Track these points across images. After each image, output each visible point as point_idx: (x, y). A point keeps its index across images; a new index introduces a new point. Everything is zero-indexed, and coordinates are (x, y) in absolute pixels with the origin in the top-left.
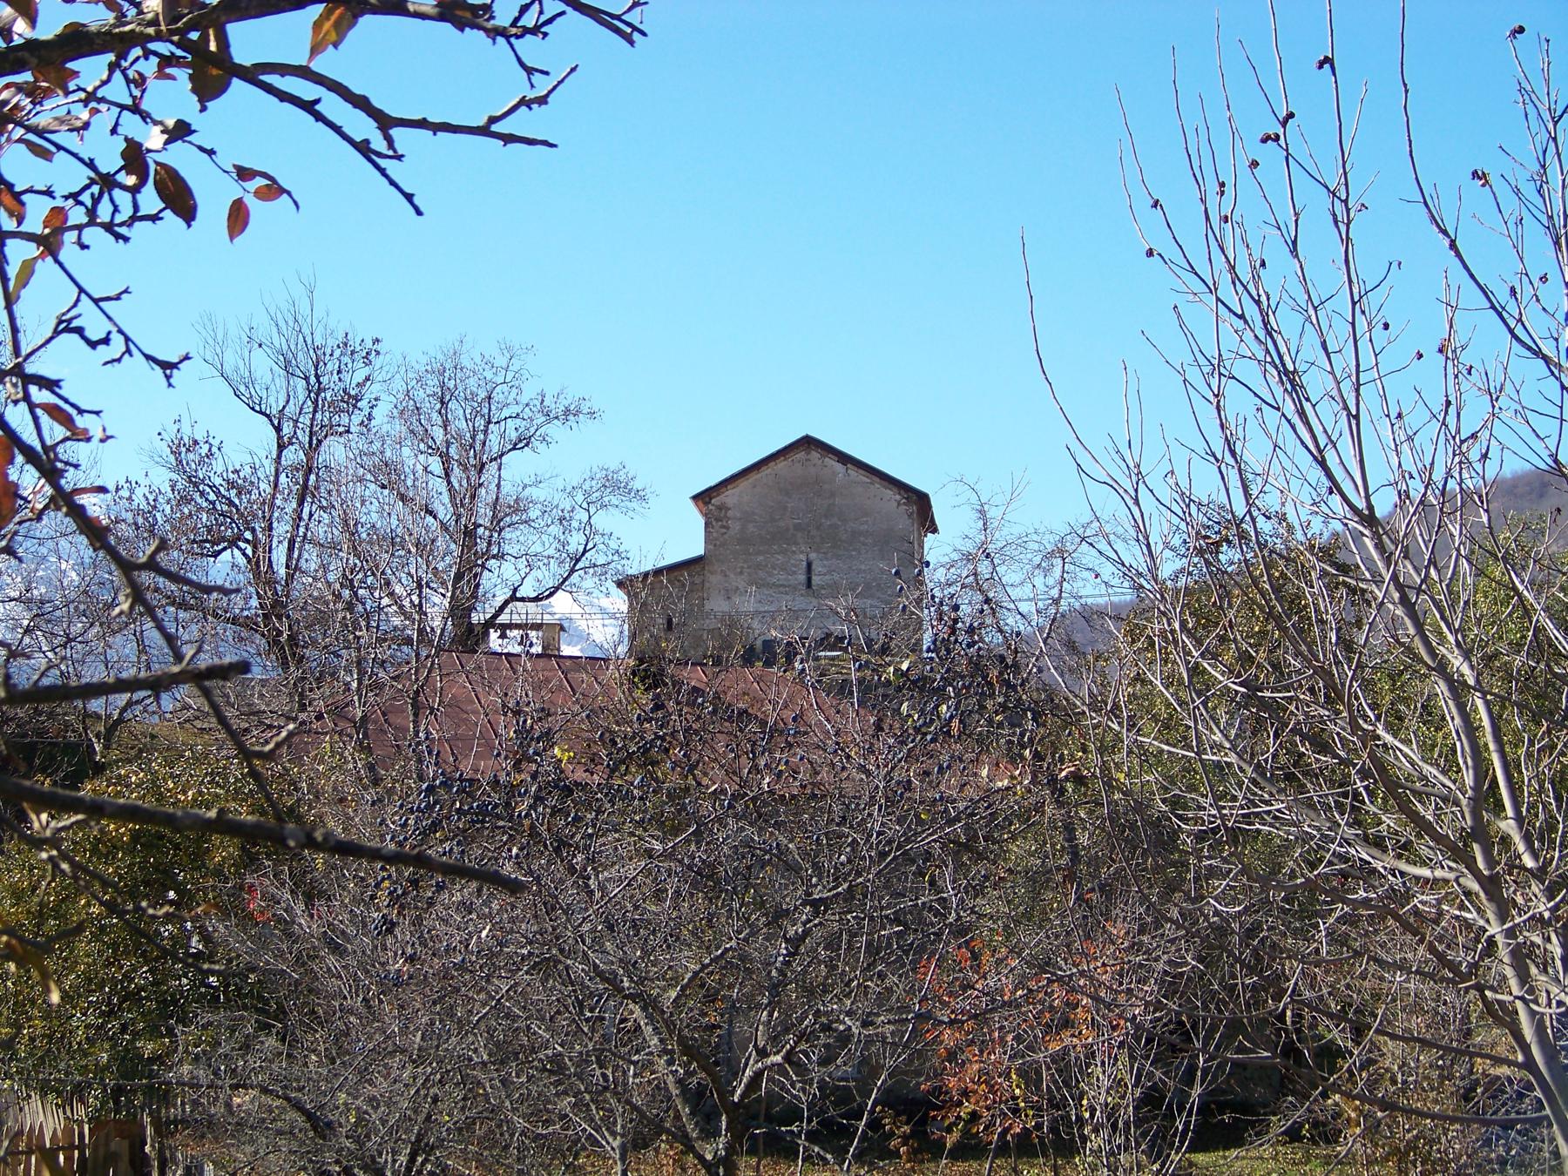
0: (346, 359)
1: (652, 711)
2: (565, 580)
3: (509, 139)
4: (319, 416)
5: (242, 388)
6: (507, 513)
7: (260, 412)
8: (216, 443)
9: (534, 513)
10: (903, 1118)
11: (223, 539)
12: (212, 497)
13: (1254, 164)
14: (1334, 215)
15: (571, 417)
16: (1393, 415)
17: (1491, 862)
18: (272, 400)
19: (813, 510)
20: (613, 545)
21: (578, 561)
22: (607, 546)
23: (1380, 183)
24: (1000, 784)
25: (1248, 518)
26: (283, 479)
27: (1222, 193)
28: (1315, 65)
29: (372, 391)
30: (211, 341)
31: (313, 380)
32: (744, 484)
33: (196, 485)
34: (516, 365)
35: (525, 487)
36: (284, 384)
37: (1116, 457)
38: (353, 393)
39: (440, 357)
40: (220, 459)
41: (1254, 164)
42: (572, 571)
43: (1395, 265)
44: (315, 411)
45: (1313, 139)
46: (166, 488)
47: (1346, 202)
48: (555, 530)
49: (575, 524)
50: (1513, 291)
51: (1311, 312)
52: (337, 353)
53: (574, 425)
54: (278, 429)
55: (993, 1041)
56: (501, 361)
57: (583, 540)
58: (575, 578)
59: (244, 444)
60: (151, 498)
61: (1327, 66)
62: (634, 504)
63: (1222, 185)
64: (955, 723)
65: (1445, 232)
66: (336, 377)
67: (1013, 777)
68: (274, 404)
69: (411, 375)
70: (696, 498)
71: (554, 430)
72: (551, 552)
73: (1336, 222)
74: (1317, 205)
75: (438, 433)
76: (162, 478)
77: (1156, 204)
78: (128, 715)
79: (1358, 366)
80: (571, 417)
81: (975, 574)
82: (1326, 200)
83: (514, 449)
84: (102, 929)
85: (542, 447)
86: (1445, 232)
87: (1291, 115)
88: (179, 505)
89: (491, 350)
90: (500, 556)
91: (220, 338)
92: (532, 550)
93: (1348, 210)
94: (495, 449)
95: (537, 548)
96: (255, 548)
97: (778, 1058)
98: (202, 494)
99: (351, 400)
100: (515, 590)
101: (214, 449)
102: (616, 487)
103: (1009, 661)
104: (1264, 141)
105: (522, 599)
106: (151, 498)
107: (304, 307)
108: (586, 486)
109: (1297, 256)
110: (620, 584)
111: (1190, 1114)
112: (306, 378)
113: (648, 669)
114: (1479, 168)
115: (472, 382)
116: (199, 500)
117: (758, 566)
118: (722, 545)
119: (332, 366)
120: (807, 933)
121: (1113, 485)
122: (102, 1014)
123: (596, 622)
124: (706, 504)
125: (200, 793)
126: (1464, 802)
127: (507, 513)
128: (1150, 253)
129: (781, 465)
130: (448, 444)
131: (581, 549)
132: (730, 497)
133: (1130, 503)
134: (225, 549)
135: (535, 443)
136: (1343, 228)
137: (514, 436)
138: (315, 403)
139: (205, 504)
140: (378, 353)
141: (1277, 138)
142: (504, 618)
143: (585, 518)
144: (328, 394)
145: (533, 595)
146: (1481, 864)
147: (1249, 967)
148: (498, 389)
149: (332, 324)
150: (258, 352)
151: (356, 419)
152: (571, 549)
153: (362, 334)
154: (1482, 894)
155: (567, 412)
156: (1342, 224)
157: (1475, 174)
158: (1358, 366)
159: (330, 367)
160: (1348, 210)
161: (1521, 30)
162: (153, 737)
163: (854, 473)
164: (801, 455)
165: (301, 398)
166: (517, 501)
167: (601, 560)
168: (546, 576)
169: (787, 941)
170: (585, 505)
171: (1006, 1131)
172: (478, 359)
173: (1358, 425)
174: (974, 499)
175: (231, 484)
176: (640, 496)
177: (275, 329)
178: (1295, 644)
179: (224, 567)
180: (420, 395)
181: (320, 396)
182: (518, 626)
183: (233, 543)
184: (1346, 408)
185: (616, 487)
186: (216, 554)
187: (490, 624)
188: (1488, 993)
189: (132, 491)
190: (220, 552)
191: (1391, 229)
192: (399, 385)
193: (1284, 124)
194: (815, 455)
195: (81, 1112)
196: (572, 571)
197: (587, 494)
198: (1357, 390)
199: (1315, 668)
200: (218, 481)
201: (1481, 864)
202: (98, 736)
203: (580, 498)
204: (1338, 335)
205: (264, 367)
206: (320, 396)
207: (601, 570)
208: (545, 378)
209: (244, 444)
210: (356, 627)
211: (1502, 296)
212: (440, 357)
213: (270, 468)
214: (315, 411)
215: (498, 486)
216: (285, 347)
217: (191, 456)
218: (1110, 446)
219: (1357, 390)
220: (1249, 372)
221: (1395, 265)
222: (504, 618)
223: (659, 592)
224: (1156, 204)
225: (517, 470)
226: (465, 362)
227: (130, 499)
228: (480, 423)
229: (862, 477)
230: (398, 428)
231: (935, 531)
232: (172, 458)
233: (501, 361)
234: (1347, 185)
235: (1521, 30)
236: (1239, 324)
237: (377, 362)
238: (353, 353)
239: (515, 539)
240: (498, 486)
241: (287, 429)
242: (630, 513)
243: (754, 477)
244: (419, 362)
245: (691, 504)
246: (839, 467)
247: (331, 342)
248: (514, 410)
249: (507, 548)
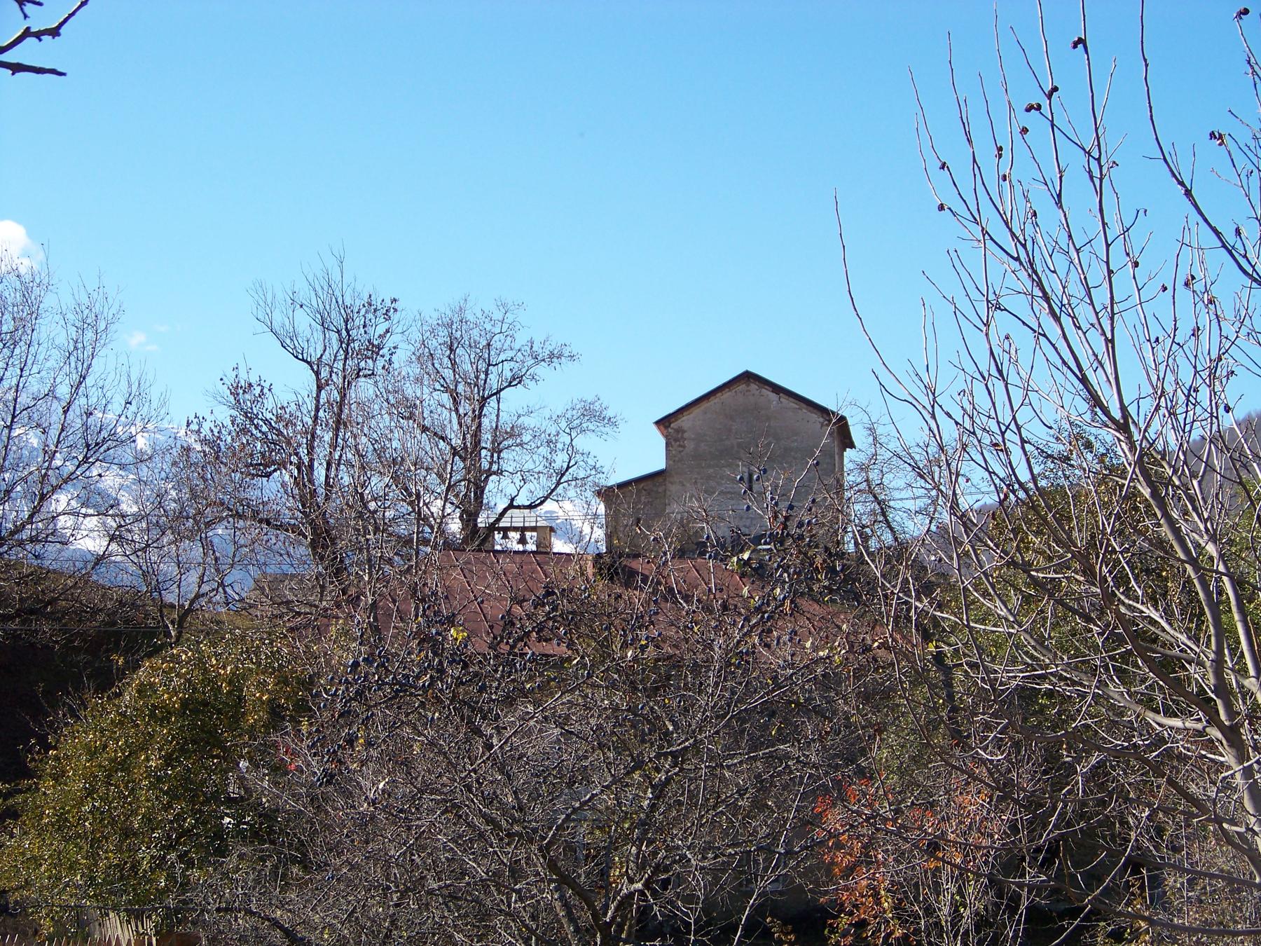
0: (370, 316)
1: (544, 597)
2: (553, 491)
3: (17, 68)
4: (349, 362)
5: (288, 341)
6: (506, 437)
7: (303, 360)
8: (267, 385)
9: (526, 438)
10: (790, 927)
11: (274, 463)
12: (265, 429)
13: (1024, 131)
14: (1090, 172)
15: (555, 360)
16: (1153, 340)
17: (1232, 713)
18: (311, 350)
19: (749, 430)
20: (591, 462)
21: (563, 475)
22: (586, 463)
23: (1128, 145)
24: (821, 654)
25: (1013, 426)
26: (321, 414)
27: (1000, 156)
28: (1071, 45)
29: (390, 342)
30: (262, 303)
31: (344, 333)
32: (696, 411)
33: (251, 420)
34: (510, 318)
35: (519, 416)
36: (322, 337)
37: (916, 379)
38: (376, 343)
39: (449, 313)
40: (271, 399)
41: (1024, 131)
42: (558, 483)
43: (1141, 213)
44: (346, 359)
45: (1072, 109)
46: (228, 422)
47: (1098, 160)
48: (544, 451)
49: (560, 446)
50: (1238, 232)
51: (1074, 254)
52: (363, 312)
53: (558, 366)
54: (317, 373)
55: (877, 862)
56: (498, 315)
57: (566, 458)
58: (560, 489)
59: (290, 386)
60: (216, 431)
61: (1081, 46)
62: (607, 429)
63: (1000, 149)
64: (788, 602)
65: (1181, 183)
66: (362, 330)
67: (831, 649)
68: (314, 352)
69: (425, 328)
70: (658, 423)
71: (541, 370)
72: (541, 468)
73: (1091, 177)
74: (1075, 161)
75: (448, 374)
76: (224, 415)
77: (943, 166)
78: (196, 606)
79: (1112, 298)
80: (555, 360)
81: (867, 480)
82: (1083, 159)
83: (510, 385)
84: (159, 779)
85: (531, 384)
86: (1181, 183)
87: (1055, 89)
88: (238, 435)
89: (490, 307)
90: (500, 472)
91: (269, 302)
92: (526, 467)
93: (1101, 167)
94: (495, 387)
95: (530, 465)
96: (299, 469)
97: (639, 886)
98: (256, 428)
99: (374, 349)
100: (512, 500)
101: (266, 391)
102: (592, 415)
103: (833, 551)
104: (1028, 110)
105: (519, 507)
106: (216, 431)
107: (336, 276)
108: (569, 415)
109: (1061, 207)
110: (599, 493)
111: (1018, 924)
112: (338, 332)
113: (615, 566)
114: (1216, 130)
115: (475, 333)
116: (254, 432)
117: (709, 477)
118: (680, 461)
119: (359, 321)
120: (668, 780)
121: (913, 402)
122: (163, 847)
123: (579, 525)
124: (666, 427)
125: (237, 668)
126: (1208, 664)
127: (506, 437)
128: (941, 207)
129: (726, 395)
130: (457, 383)
131: (565, 466)
132: (685, 422)
133: (928, 417)
134: (275, 470)
135: (526, 381)
136: (1097, 182)
137: (509, 375)
138: (346, 352)
139: (259, 435)
140: (395, 310)
141: (1039, 108)
142: (504, 523)
143: (568, 440)
144: (357, 344)
145: (527, 503)
146: (1223, 716)
147: (1024, 806)
148: (496, 338)
149: (359, 288)
150: (299, 311)
151: (381, 362)
152: (557, 465)
153: (383, 295)
154: (1224, 742)
155: (551, 356)
156: (1097, 181)
157: (1212, 135)
158: (1112, 298)
159: (357, 322)
160: (1101, 167)
161: (1246, 12)
162: (218, 623)
163: (785, 400)
164: (742, 387)
165: (336, 348)
166: (512, 428)
167: (582, 474)
168: (537, 488)
169: (653, 787)
170: (568, 430)
171: (888, 935)
172: (479, 314)
173: (1113, 348)
174: (866, 419)
175: (279, 418)
176: (611, 422)
177: (313, 294)
178: (1054, 532)
179: (273, 489)
180: (433, 343)
181: (351, 344)
182: (515, 529)
183: (282, 465)
184: (1104, 333)
185: (592, 415)
186: (268, 475)
187: (492, 528)
188: (1225, 825)
189: (200, 425)
190: (271, 474)
191: (1138, 182)
192: (416, 336)
193: (1050, 96)
194: (754, 387)
195: (149, 925)
196: (558, 483)
197: (570, 421)
198: (1112, 319)
199: (1073, 552)
200: (269, 416)
201: (1223, 716)
202: (173, 622)
203: (563, 424)
204: (1096, 275)
205: (304, 323)
206: (351, 344)
207: (581, 482)
208: (533, 329)
209: (290, 386)
210: (366, 532)
211: (1230, 238)
212: (449, 313)
213: (311, 405)
214: (346, 359)
215: (498, 416)
216: (321, 307)
217: (247, 396)
218: (911, 370)
219: (1112, 319)
220: (1019, 304)
221: (1141, 213)
222: (504, 523)
223: (629, 499)
224: (943, 166)
225: (513, 400)
226: (470, 317)
227: (198, 432)
228: (482, 366)
229: (792, 404)
230: (415, 370)
231: (852, 446)
232: (232, 398)
233: (498, 315)
234: (1099, 145)
235: (1246, 12)
236: (1015, 265)
237: (395, 317)
238: (375, 310)
239: (511, 460)
240: (498, 416)
241: (324, 373)
242: (604, 436)
243: (705, 405)
244: (432, 318)
245: (654, 428)
246: (773, 396)
247: (358, 303)
248: (510, 354)
249: (505, 466)
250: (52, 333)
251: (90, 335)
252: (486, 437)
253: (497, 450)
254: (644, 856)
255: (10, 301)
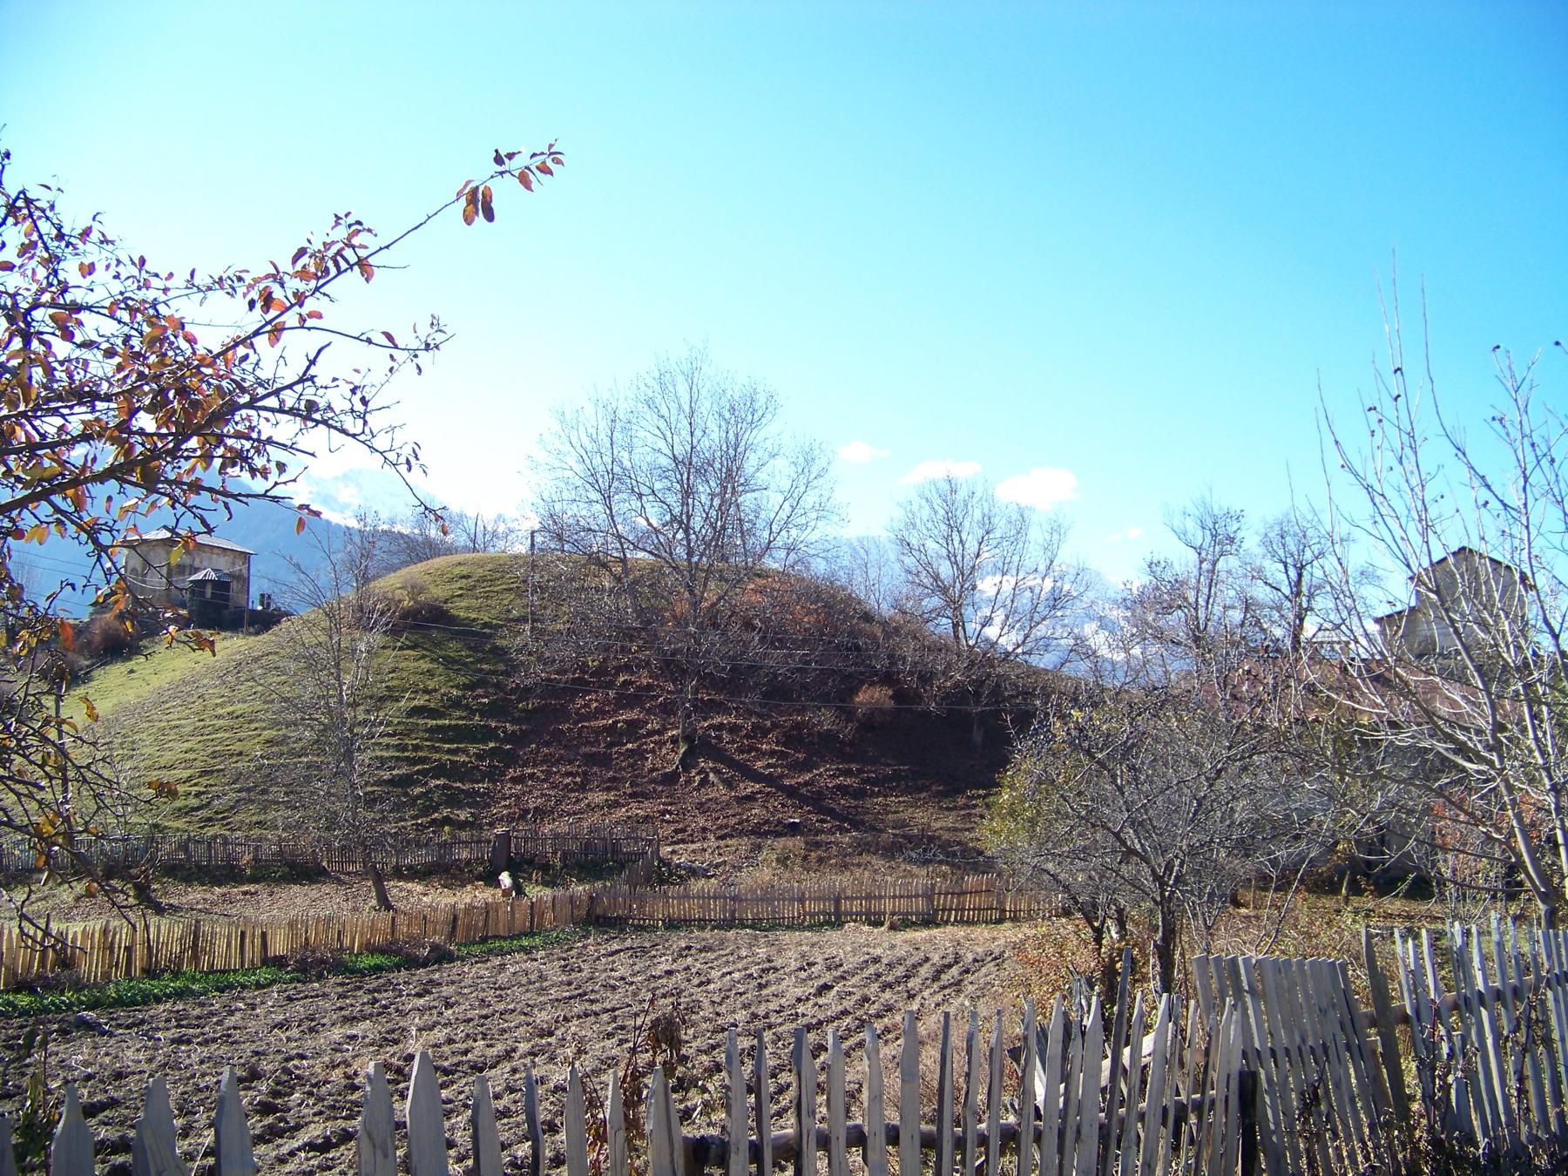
29: (1240, 535)
59: (1183, 561)
75: (1281, 552)
153: (1235, 508)
180: (1272, 535)
181: (1219, 538)
205: (1191, 526)
209: (1183, 561)
213: (1196, 572)
230: (1262, 550)
250: (1036, 536)
251: (1056, 536)
252: (1304, 589)
253: (1311, 596)
254: (490, 636)
255: (323, 639)
